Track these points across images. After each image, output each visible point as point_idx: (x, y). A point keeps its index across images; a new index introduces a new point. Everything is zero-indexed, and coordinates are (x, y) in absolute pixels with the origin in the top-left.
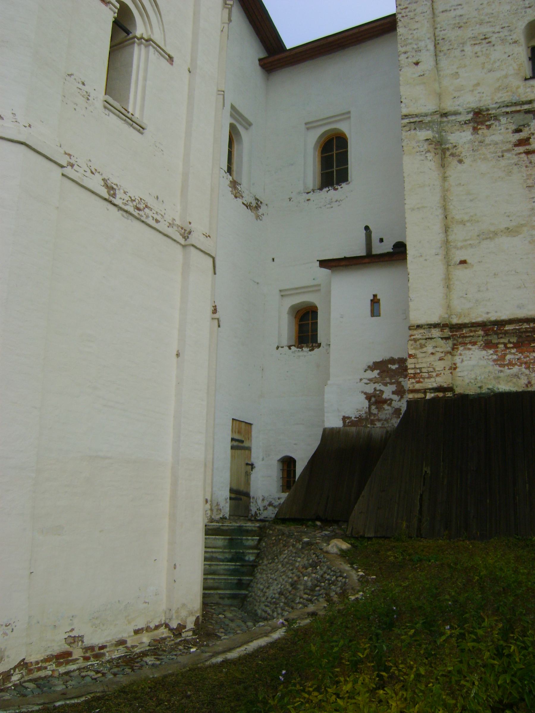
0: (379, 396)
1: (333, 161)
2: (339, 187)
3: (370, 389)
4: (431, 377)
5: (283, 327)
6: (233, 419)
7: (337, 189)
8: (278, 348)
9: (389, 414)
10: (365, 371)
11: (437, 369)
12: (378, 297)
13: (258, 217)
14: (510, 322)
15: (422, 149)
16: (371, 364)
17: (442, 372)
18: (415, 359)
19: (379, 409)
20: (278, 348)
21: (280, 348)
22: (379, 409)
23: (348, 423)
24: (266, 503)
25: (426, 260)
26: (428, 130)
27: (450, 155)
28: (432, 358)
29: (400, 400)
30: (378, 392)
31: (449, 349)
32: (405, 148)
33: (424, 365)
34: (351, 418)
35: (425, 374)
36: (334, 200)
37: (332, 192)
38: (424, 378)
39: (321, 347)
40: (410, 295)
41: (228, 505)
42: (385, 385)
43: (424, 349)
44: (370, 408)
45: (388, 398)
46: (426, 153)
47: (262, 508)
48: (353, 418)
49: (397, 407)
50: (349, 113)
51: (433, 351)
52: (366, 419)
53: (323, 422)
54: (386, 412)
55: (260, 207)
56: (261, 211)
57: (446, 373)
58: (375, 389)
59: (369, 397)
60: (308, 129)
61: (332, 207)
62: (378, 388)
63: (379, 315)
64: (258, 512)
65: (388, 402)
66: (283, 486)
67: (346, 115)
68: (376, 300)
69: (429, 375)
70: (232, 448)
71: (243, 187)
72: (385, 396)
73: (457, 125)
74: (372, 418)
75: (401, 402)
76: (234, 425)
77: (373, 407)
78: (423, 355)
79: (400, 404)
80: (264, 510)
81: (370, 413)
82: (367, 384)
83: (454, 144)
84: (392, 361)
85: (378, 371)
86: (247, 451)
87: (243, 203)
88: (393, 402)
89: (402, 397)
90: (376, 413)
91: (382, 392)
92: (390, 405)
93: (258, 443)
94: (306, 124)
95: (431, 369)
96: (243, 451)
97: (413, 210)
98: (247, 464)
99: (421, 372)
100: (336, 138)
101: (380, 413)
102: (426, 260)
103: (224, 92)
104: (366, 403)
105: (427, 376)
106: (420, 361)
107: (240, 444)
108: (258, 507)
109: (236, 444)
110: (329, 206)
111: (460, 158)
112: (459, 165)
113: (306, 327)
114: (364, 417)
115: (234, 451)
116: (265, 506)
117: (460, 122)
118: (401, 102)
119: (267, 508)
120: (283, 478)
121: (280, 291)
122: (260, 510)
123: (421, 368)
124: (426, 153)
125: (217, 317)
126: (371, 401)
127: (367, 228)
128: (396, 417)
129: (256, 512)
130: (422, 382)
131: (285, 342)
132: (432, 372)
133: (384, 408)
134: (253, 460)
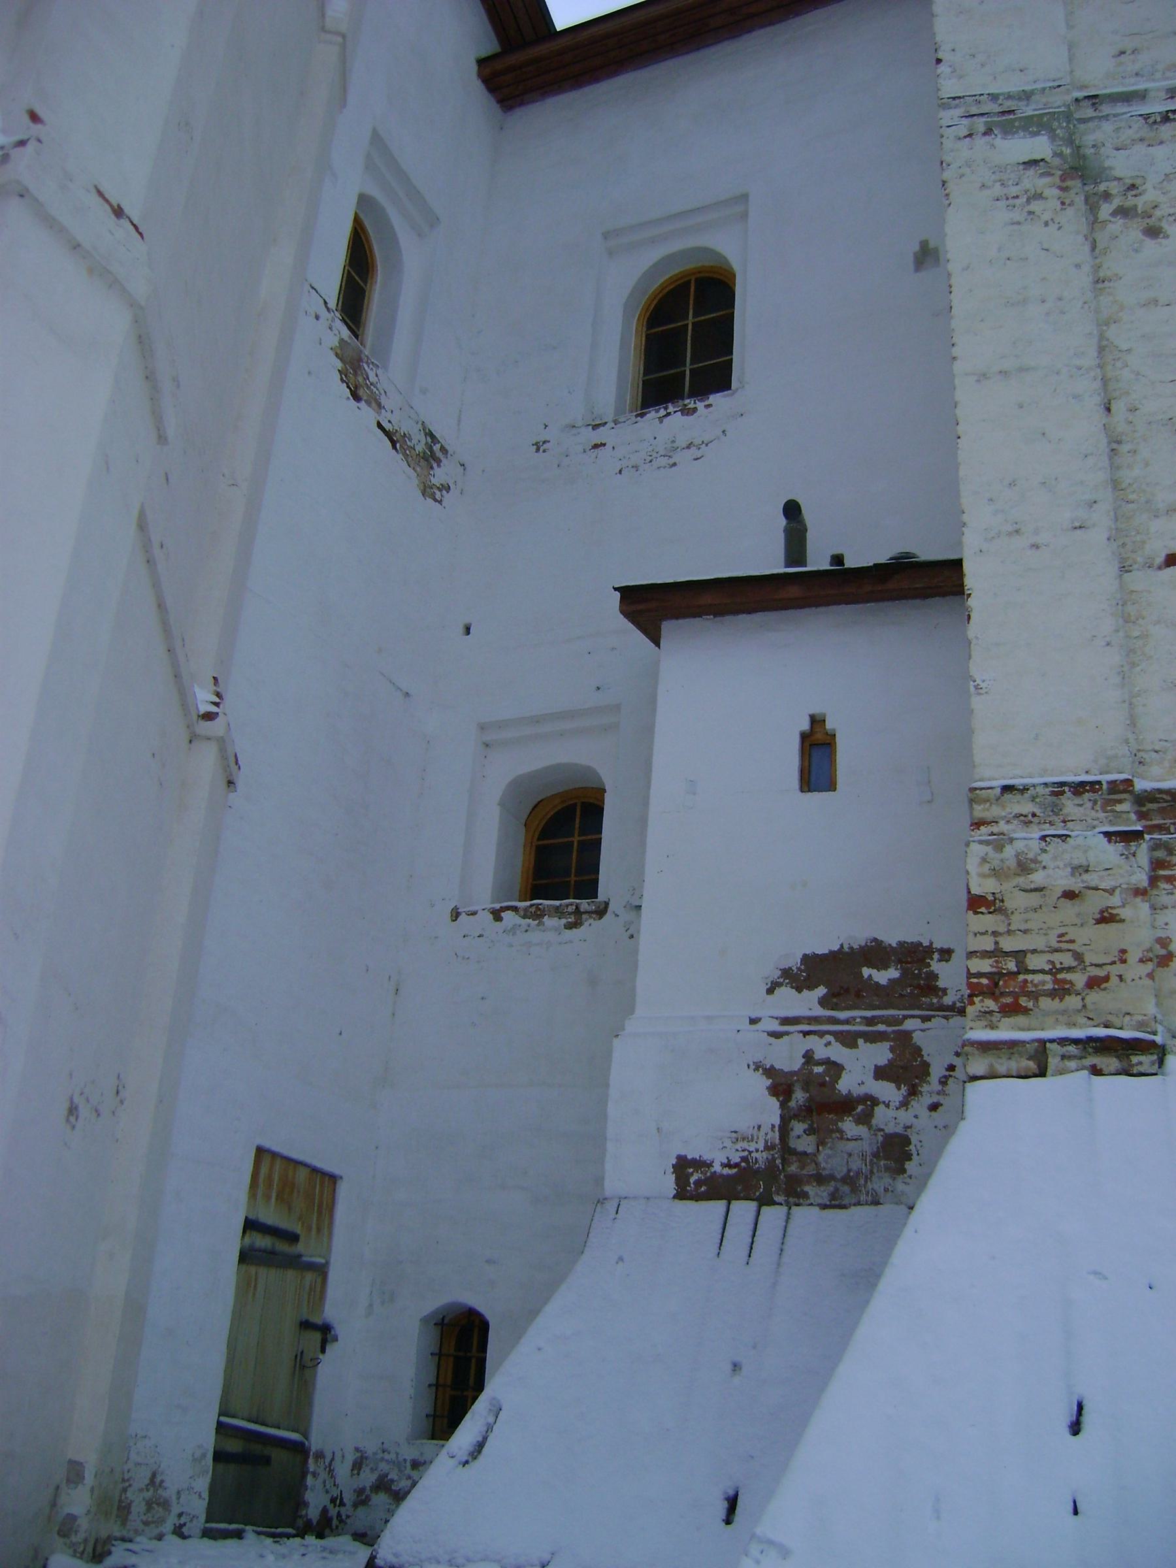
0: (823, 1084)
1: (686, 338)
2: (700, 406)
3: (787, 1055)
4: (1068, 992)
5: (479, 847)
6: (260, 1151)
7: (695, 410)
8: (456, 915)
9: (863, 1156)
10: (770, 991)
11: (1089, 958)
12: (829, 725)
13: (428, 491)
14: (288, 1536)
15: (1014, 191)
16: (794, 962)
17: (1115, 970)
18: (999, 917)
19: (822, 1134)
20: (456, 915)
21: (463, 917)
22: (822, 1134)
23: (698, 1183)
24: (368, 1478)
25: (1036, 546)
26: (1037, 134)
27: (1115, 213)
28: (1069, 910)
29: (904, 1104)
30: (819, 1069)
31: (1141, 878)
32: (951, 186)
33: (1039, 942)
34: (710, 1165)
35: (1037, 978)
36: (682, 442)
37: (677, 419)
38: (1035, 996)
39: (608, 917)
40: (974, 670)
41: (203, 1484)
42: (849, 1040)
43: (1038, 878)
44: (784, 1129)
45: (858, 1091)
46: (1028, 201)
47: (349, 1498)
48: (717, 1168)
49: (890, 1129)
50: (745, 198)
51: (1075, 884)
52: (771, 1171)
53: (599, 1181)
54: (851, 1145)
55: (439, 462)
56: (440, 475)
57: (1128, 976)
58: (808, 1056)
59: (781, 1086)
60: (611, 253)
61: (675, 464)
62: (821, 1053)
63: (831, 786)
64: (333, 1512)
65: (861, 1107)
66: (435, 1416)
67: (738, 204)
68: (819, 736)
69: (1056, 981)
70: (246, 1257)
71: (391, 377)
72: (845, 1085)
73: (1135, 126)
74: (793, 1168)
75: (911, 1112)
76: (264, 1170)
77: (798, 1127)
78: (1034, 899)
79: (904, 1116)
80: (355, 1505)
81: (785, 1148)
82: (776, 1035)
83: (1129, 182)
84: (876, 953)
85: (821, 991)
86: (309, 1277)
87: (379, 425)
88: (879, 1110)
89: (913, 1092)
90: (810, 1150)
91: (835, 1069)
92: (865, 1119)
93: (354, 1247)
94: (606, 236)
95: (1067, 960)
96: (290, 1274)
97: (983, 377)
98: (306, 1325)
99: (1023, 969)
100: (699, 282)
101: (825, 1152)
102: (1036, 546)
103: (344, 36)
104: (771, 1113)
105: (1049, 986)
106: (1017, 922)
107: (283, 1247)
108: (335, 1492)
109: (262, 1242)
110: (664, 461)
111: (1151, 222)
112: (1149, 243)
113: (561, 849)
114: (761, 1164)
115: (253, 1269)
116: (360, 1491)
117: (1146, 117)
118: (939, 61)
119: (368, 1498)
120: (437, 1386)
121: (482, 727)
122: (342, 1504)
123: (1023, 953)
124: (1028, 201)
125: (221, 732)
126: (792, 1104)
127: (792, 510)
128: (887, 1169)
129: (325, 1511)
130: (1026, 1011)
131: (483, 894)
132: (1070, 969)
133: (841, 1132)
134: (331, 1312)
